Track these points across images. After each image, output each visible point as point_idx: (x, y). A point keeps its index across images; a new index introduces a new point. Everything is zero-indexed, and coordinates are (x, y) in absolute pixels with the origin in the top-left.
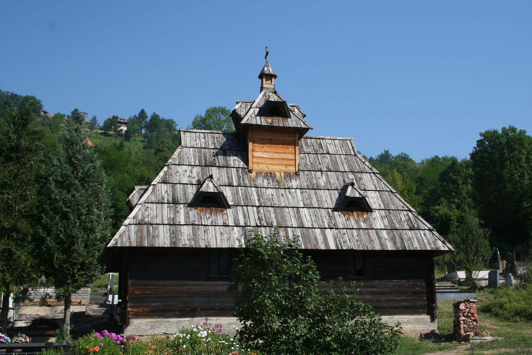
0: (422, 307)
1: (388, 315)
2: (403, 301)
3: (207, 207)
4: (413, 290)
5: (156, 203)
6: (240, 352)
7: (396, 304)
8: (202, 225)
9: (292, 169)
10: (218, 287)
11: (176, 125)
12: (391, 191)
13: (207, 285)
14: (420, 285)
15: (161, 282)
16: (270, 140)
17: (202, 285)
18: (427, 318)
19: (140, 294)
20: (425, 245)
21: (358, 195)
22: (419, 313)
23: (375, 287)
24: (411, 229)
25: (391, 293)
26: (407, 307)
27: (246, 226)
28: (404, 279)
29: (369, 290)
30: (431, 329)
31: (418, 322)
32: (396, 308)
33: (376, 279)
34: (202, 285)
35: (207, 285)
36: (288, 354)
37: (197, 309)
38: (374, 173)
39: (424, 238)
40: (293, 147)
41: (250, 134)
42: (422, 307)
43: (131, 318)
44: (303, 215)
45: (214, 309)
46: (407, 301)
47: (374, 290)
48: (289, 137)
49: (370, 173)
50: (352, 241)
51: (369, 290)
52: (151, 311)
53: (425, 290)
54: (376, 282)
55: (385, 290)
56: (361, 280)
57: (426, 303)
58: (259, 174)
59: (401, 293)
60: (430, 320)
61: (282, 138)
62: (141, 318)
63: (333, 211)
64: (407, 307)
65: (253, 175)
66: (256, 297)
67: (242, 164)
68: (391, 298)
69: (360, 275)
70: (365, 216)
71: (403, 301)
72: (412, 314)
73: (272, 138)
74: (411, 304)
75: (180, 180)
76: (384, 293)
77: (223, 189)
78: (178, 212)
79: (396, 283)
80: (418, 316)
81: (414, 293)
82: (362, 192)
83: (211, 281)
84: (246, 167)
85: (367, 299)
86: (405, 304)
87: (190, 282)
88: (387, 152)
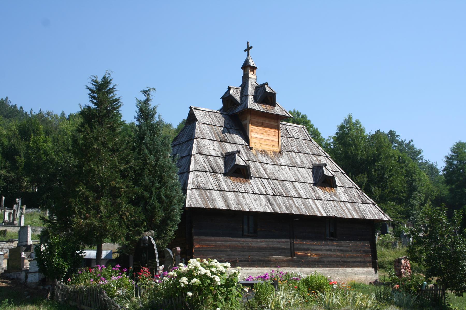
0: (369, 262)
1: (350, 268)
2: (358, 257)
3: (237, 177)
4: (363, 249)
5: (201, 171)
6: (48, 309)
7: (354, 260)
9: (276, 149)
10: (250, 243)
11: (405, 141)
12: (342, 172)
13: (242, 241)
14: (368, 244)
15: (212, 238)
16: (262, 123)
17: (239, 241)
18: (373, 270)
19: (199, 248)
20: (314, 211)
21: (331, 175)
22: (367, 267)
24: (363, 203)
25: (351, 251)
26: (360, 262)
27: (267, 194)
28: (358, 241)
29: (338, 248)
30: (375, 278)
31: (368, 273)
32: (354, 262)
34: (239, 241)
35: (242, 241)
36: (465, 285)
37: (236, 261)
38: (327, 157)
39: (372, 211)
40: (276, 131)
41: (249, 117)
42: (369, 262)
44: (296, 187)
45: (248, 261)
46: (361, 257)
47: (342, 248)
49: (324, 156)
50: (319, 209)
51: (338, 248)
53: (370, 249)
54: (343, 242)
55: (348, 249)
56: (334, 240)
57: (370, 259)
58: (257, 151)
59: (357, 251)
60: (374, 272)
61: (270, 123)
63: (314, 186)
65: (254, 151)
67: (243, 142)
69: (334, 236)
70: (333, 191)
71: (358, 257)
72: (364, 267)
73: (264, 122)
74: (362, 260)
75: (210, 153)
76: (347, 251)
77: (250, 163)
78: (219, 180)
79: (353, 244)
80: (368, 269)
81: (364, 251)
82: (333, 173)
83: (244, 238)
84: (247, 144)
85: (338, 255)
86: (359, 259)
87: (231, 239)
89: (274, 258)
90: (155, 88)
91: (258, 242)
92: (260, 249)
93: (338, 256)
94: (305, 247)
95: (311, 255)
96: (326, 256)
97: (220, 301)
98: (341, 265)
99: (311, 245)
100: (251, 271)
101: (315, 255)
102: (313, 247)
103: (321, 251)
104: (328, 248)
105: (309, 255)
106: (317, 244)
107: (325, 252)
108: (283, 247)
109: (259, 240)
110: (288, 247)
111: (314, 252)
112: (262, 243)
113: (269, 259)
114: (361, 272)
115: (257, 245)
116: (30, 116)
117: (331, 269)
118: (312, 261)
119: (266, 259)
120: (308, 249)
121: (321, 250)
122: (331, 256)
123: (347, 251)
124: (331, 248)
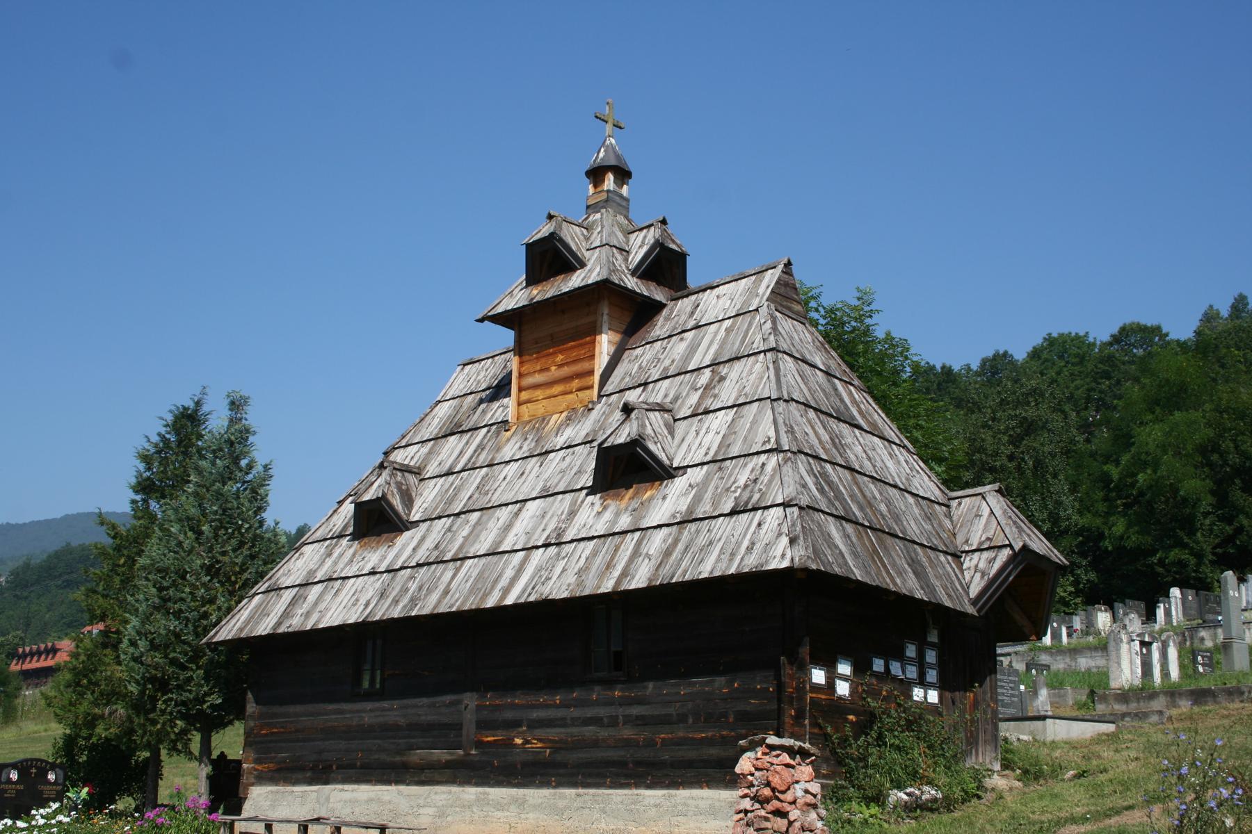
4: (741, 707)
7: (691, 754)
8: (801, 508)
13: (350, 712)
23: (649, 703)
25: (682, 719)
29: (636, 711)
32: (689, 764)
33: (650, 679)
35: (350, 712)
43: (253, 784)
48: (600, 343)
51: (636, 711)
52: (279, 770)
55: (671, 710)
62: (691, 788)
64: (689, 764)
66: (814, 724)
68: (681, 734)
69: (625, 669)
71: (709, 742)
73: (439, 459)
76: (664, 721)
79: (697, 688)
88: (68, 544)
89: (418, 755)
90: (632, 167)
91: (384, 710)
92: (387, 730)
93: (627, 743)
94: (509, 715)
95: (527, 742)
96: (581, 744)
97: (71, 704)
98: (627, 776)
99: (533, 707)
100: (355, 794)
101: (540, 740)
102: (535, 714)
103: (565, 726)
104: (590, 712)
105: (518, 741)
106: (551, 703)
107: (575, 730)
108: (445, 720)
109: (386, 704)
110: (1003, 726)
111: (540, 732)
112: (393, 711)
113: (405, 759)
114: (703, 805)
115: (381, 720)
116: (22, 787)
117: (581, 791)
118: (525, 764)
119: (398, 759)
120: (515, 724)
121: (561, 722)
122: (595, 744)
123: (664, 721)
124: (602, 712)
